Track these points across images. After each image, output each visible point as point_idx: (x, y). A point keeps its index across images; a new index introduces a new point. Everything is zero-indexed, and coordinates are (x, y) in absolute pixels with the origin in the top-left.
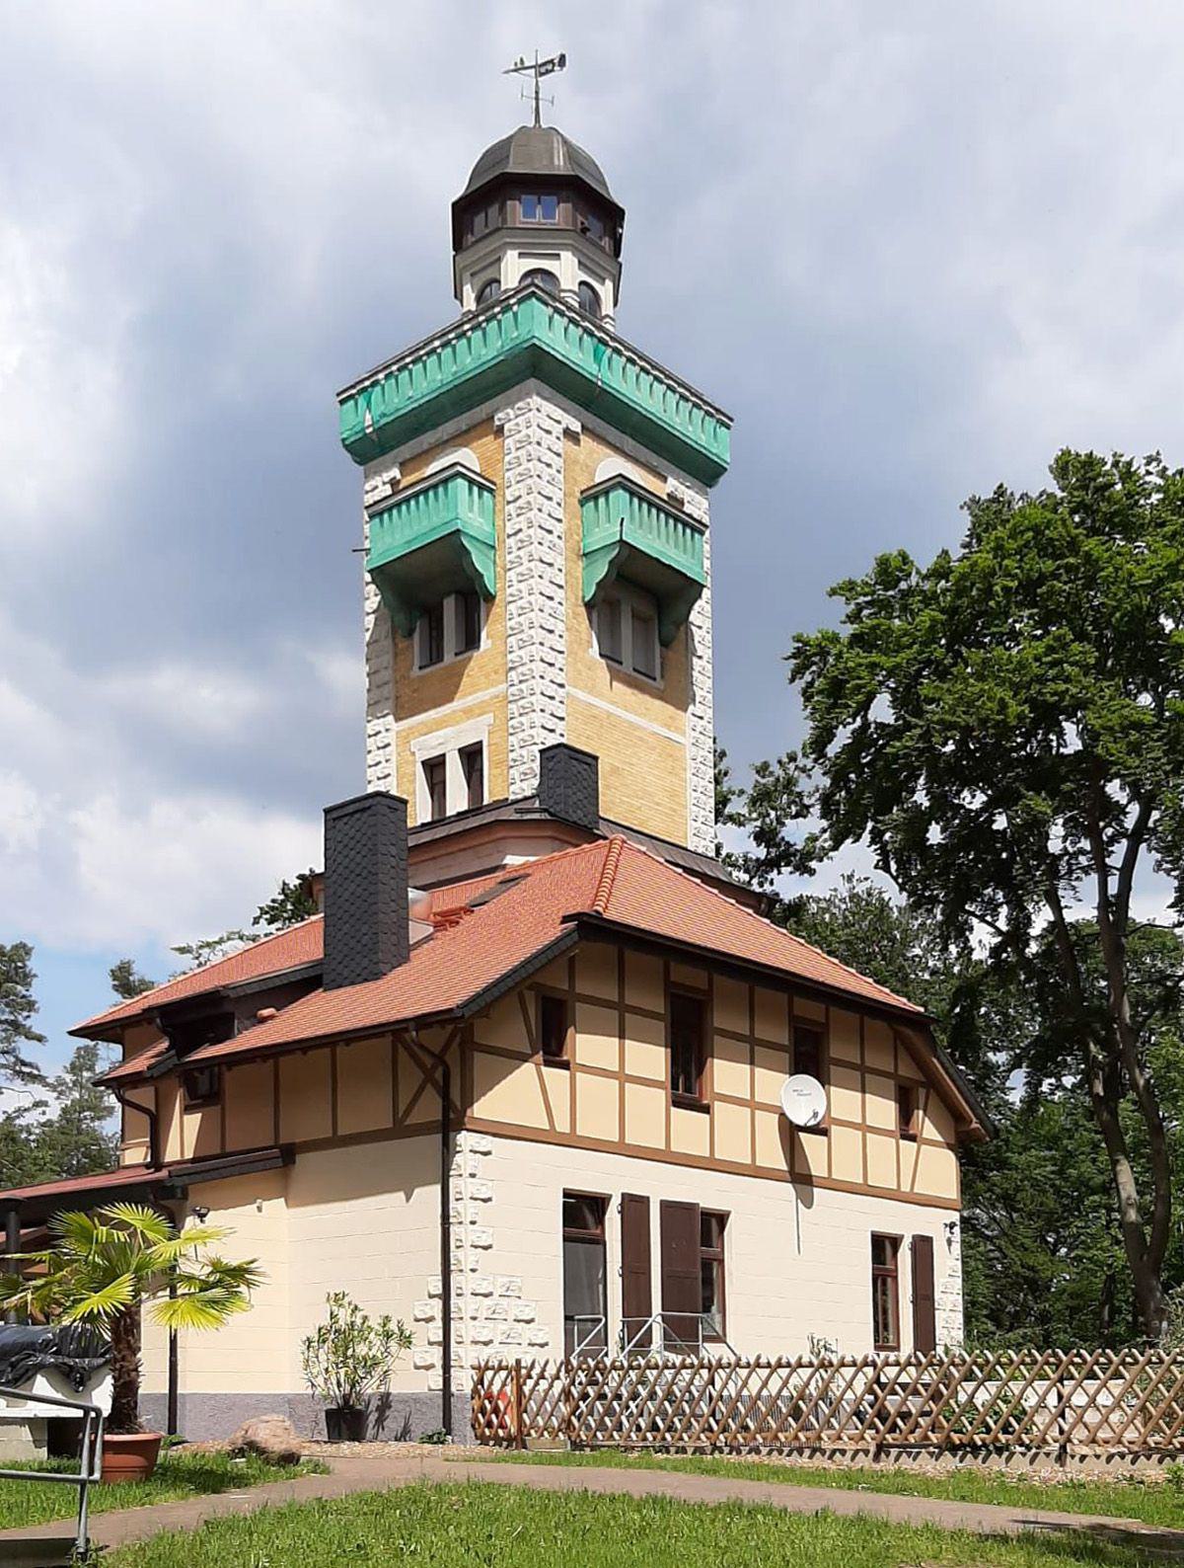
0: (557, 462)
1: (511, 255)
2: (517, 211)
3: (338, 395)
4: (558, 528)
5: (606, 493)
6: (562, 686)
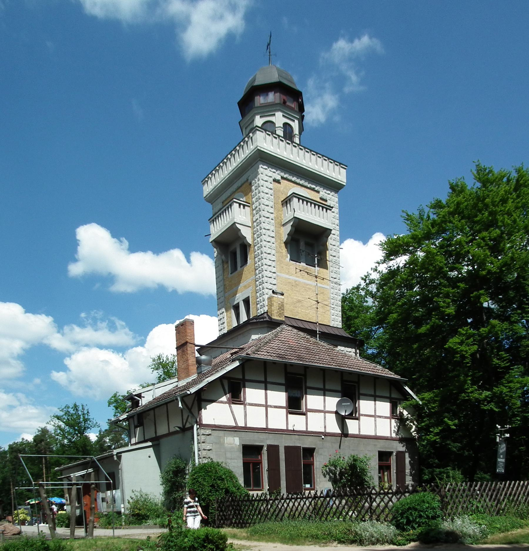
0: (271, 192)
1: (257, 118)
2: (260, 100)
3: (202, 182)
4: (272, 216)
5: (290, 200)
6: (274, 273)
